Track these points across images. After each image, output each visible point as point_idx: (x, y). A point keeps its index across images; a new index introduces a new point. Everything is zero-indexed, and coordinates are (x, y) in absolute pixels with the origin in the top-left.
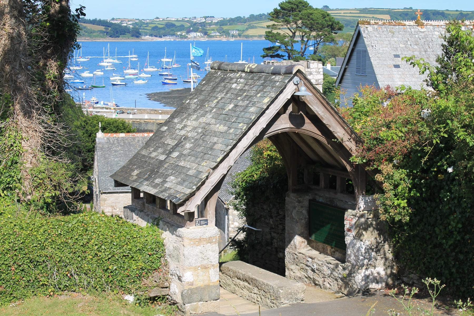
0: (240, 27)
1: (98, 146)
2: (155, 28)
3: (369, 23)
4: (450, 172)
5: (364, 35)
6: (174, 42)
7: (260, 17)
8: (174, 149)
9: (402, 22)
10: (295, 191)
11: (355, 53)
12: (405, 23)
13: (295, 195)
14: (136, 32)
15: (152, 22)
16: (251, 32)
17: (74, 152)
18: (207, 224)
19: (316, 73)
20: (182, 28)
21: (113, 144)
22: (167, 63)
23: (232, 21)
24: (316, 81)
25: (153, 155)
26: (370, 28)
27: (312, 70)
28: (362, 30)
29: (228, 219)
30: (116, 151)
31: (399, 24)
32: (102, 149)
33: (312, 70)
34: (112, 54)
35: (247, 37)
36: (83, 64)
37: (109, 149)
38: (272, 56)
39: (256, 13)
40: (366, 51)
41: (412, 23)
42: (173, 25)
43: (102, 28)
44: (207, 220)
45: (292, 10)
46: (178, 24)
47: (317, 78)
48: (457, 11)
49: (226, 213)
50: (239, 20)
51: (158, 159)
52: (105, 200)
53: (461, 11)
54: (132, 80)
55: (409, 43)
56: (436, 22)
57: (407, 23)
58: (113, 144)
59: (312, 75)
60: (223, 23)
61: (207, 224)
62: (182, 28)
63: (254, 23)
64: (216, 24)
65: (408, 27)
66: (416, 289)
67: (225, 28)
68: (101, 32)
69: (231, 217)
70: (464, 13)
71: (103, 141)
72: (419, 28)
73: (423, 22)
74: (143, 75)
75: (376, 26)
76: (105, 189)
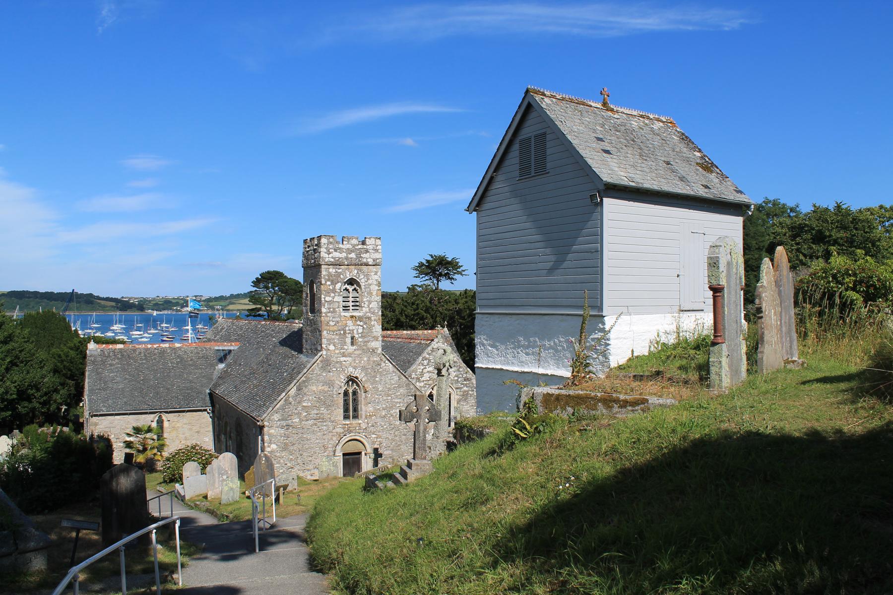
0: (223, 303)
1: (89, 359)
2: (156, 304)
4: (115, 463)
6: (171, 315)
7: (238, 296)
14: (141, 306)
15: (154, 299)
16: (231, 307)
17: (65, 375)
20: (177, 304)
21: (109, 356)
22: (167, 327)
23: (217, 299)
29: (263, 440)
30: (111, 365)
32: (94, 362)
34: (120, 322)
35: (228, 310)
36: (96, 328)
37: (103, 362)
38: (255, 316)
39: (235, 293)
42: (170, 302)
43: (113, 304)
45: (271, 279)
46: (174, 301)
49: (258, 432)
50: (221, 298)
52: (96, 424)
54: (136, 339)
58: (109, 356)
60: (210, 300)
62: (177, 304)
63: (233, 300)
64: (204, 301)
67: (211, 304)
68: (112, 307)
69: (266, 438)
71: (95, 353)
74: (146, 335)
76: (97, 411)
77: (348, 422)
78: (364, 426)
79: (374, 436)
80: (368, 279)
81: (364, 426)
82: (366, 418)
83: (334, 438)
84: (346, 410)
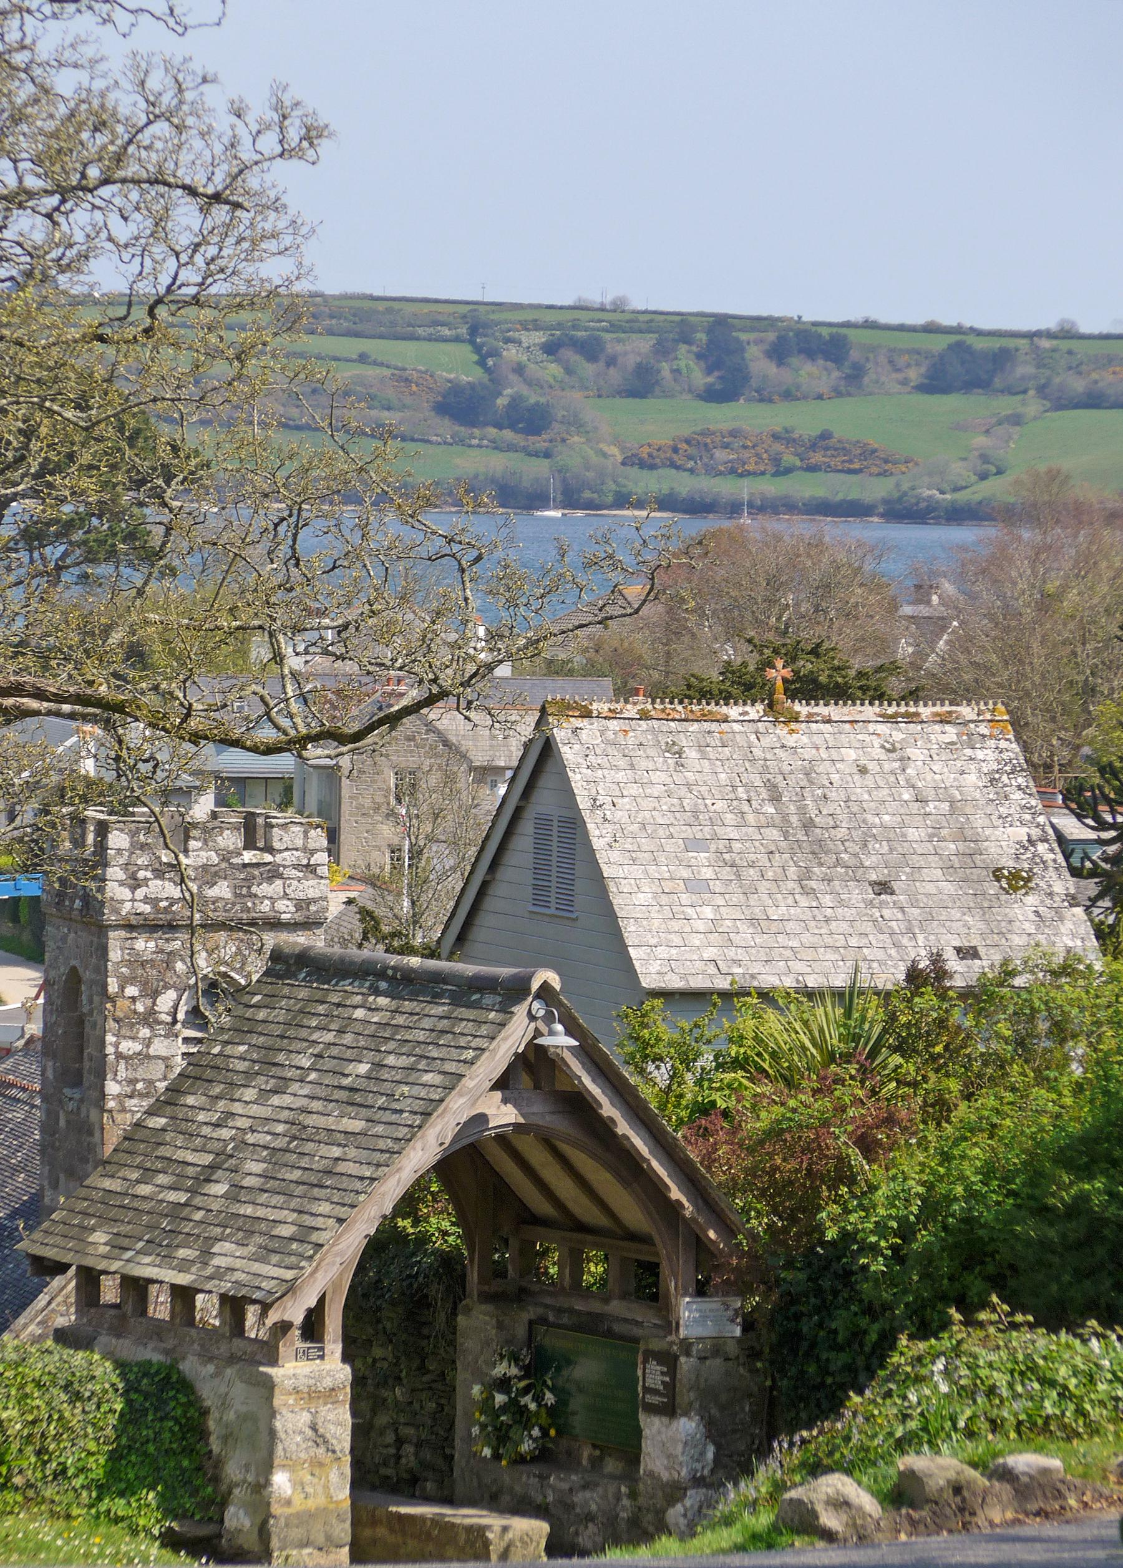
3: (587, 714)
5: (569, 754)
8: (207, 1174)
9: (712, 707)
10: (487, 1298)
11: (527, 827)
12: (724, 710)
13: (489, 1307)
18: (322, 1357)
19: (295, 873)
24: (298, 908)
25: (144, 1190)
26: (590, 730)
27: (279, 858)
28: (560, 735)
31: (704, 718)
33: (279, 858)
40: (574, 825)
41: (755, 711)
44: (322, 1349)
47: (302, 896)
48: (931, 329)
51: (162, 1201)
53: (958, 330)
55: (741, 792)
56: (845, 710)
57: (733, 712)
59: (279, 882)
61: (322, 1357)
65: (736, 727)
66: (950, 988)
70: (979, 344)
72: (782, 731)
73: (797, 707)
75: (614, 725)
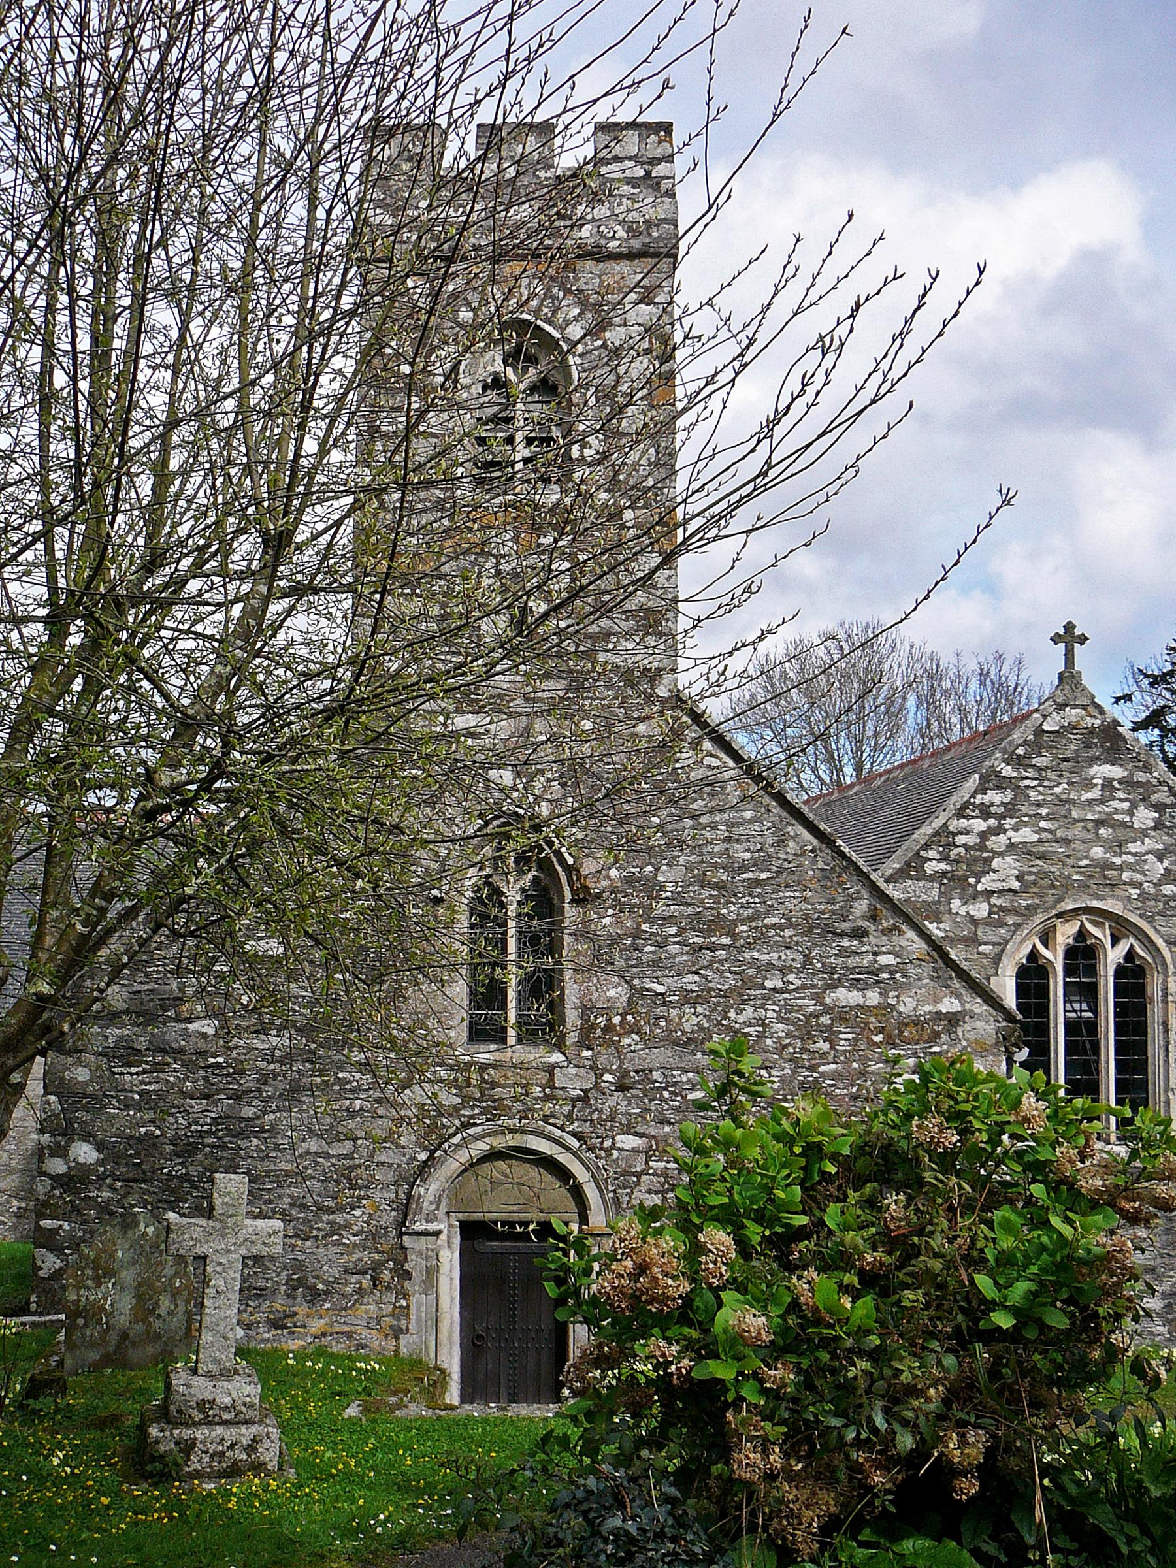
77: (486, 1054)
78: (572, 1080)
79: (628, 1142)
80: (603, 324)
81: (572, 1080)
82: (585, 1041)
83: (408, 1138)
84: (488, 995)
